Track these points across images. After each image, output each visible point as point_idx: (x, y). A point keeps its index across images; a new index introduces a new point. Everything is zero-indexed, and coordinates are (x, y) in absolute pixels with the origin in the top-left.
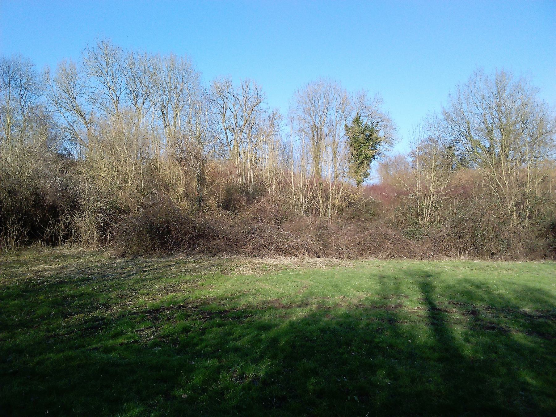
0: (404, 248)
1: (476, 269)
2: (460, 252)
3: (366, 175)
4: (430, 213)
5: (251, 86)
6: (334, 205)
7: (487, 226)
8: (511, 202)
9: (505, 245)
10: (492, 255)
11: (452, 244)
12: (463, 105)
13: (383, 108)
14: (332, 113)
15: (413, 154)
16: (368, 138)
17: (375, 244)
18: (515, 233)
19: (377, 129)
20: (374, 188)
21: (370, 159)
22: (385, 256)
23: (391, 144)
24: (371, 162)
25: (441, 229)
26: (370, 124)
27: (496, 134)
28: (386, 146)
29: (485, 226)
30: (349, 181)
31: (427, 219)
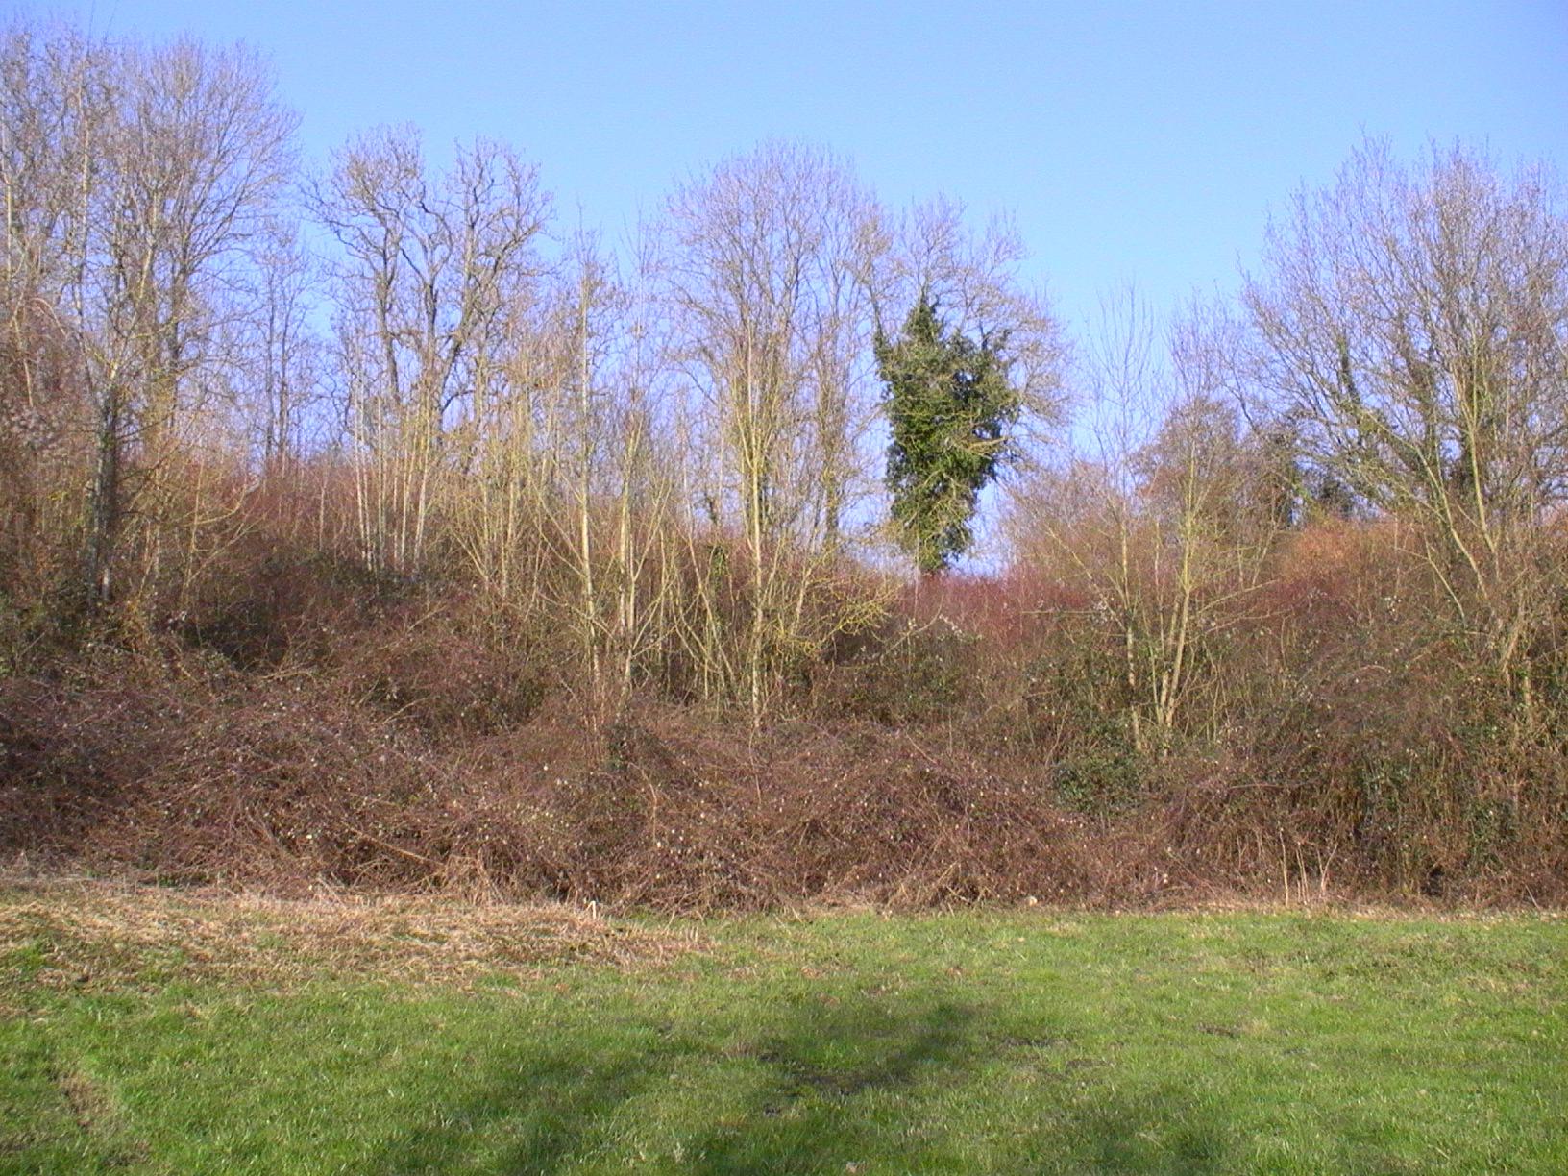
0: (1031, 850)
1: (1349, 970)
2: (1293, 869)
3: (958, 539)
4: (1179, 689)
5: (499, 169)
6: (769, 649)
7: (1416, 742)
8: (1516, 631)
9: (1490, 834)
10: (1434, 883)
11: (1257, 830)
12: (1324, 274)
13: (1023, 277)
14: (818, 290)
15: (1141, 462)
16: (966, 395)
17: (888, 832)
18: (1531, 775)
19: (1004, 356)
20: (988, 588)
21: (979, 472)
22: (928, 891)
23: (1052, 413)
24: (978, 484)
25: (1220, 756)
26: (976, 338)
27: (1450, 390)
28: (1040, 426)
29: (1406, 743)
30: (893, 565)
31: (1165, 714)
